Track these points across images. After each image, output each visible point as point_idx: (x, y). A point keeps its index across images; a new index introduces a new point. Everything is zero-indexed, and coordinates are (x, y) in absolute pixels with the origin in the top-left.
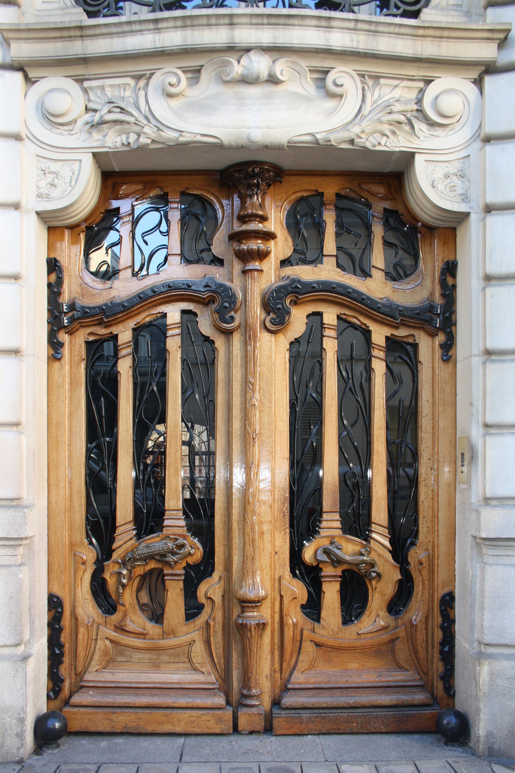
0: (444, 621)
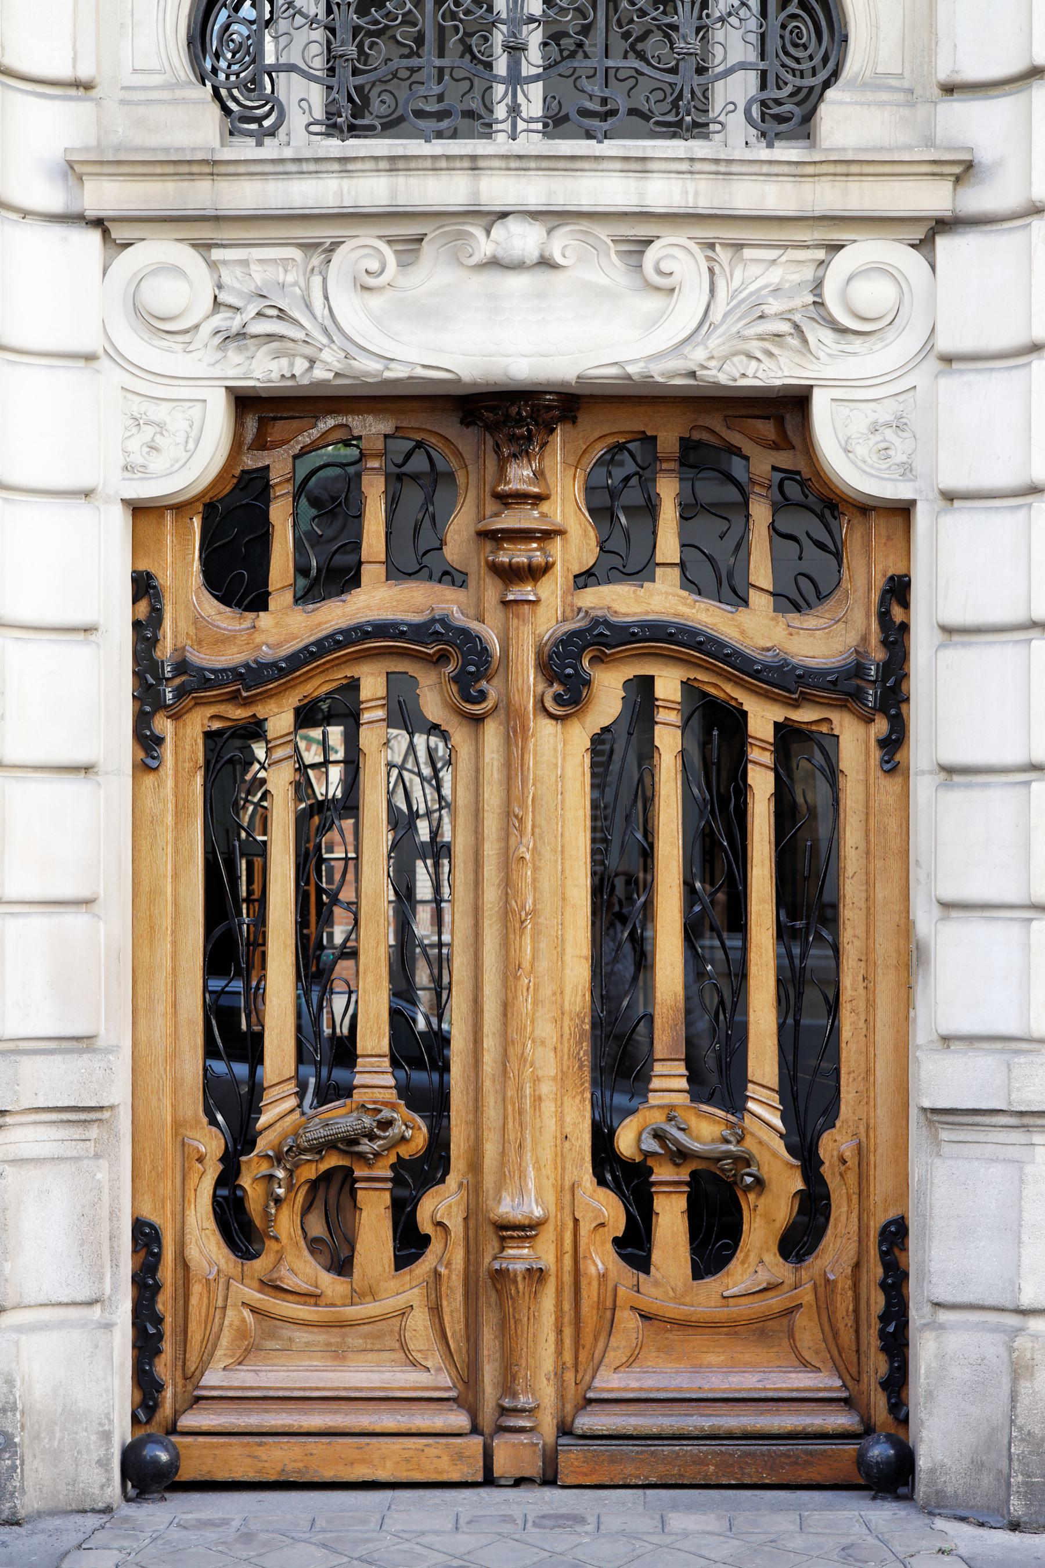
0: (886, 1275)
